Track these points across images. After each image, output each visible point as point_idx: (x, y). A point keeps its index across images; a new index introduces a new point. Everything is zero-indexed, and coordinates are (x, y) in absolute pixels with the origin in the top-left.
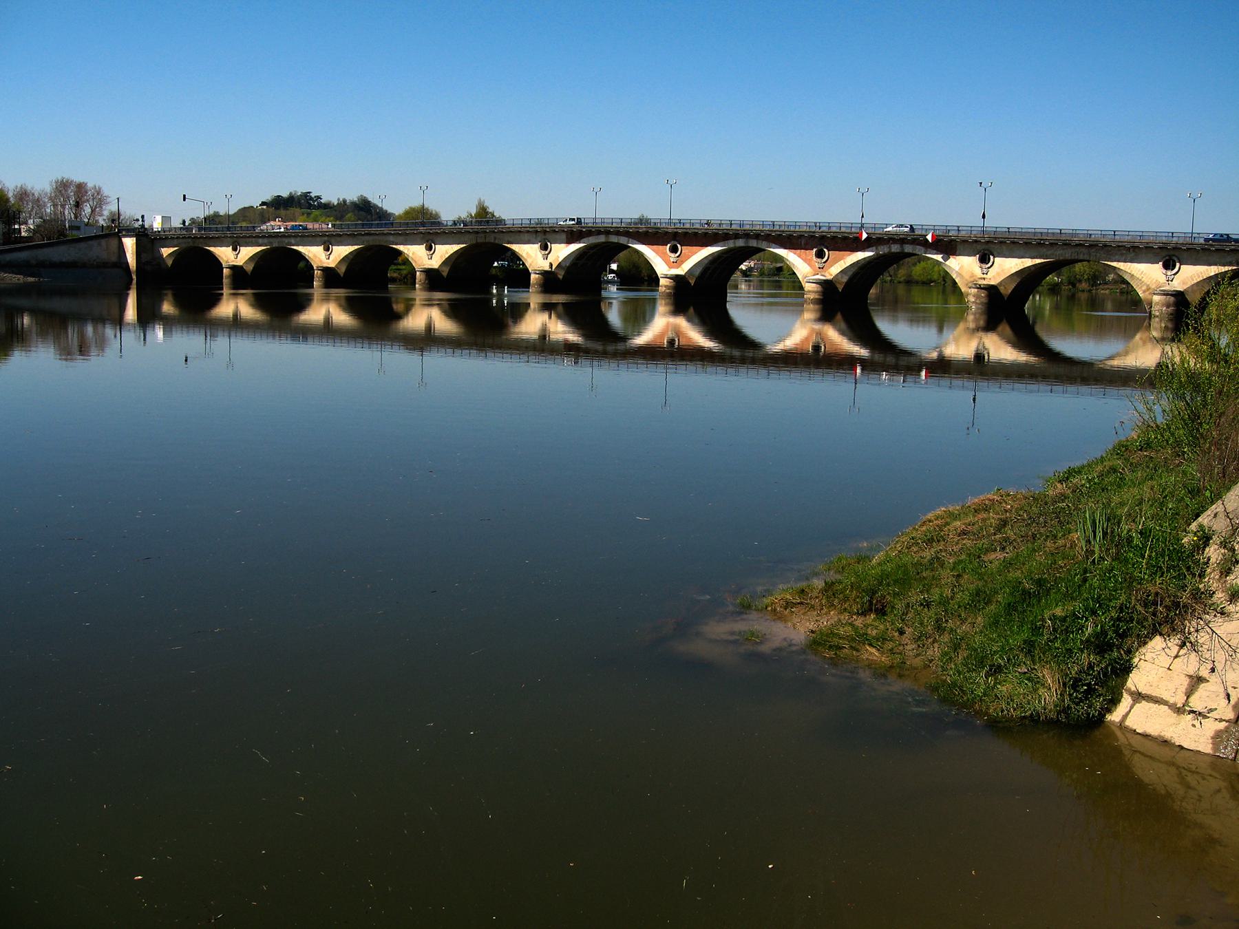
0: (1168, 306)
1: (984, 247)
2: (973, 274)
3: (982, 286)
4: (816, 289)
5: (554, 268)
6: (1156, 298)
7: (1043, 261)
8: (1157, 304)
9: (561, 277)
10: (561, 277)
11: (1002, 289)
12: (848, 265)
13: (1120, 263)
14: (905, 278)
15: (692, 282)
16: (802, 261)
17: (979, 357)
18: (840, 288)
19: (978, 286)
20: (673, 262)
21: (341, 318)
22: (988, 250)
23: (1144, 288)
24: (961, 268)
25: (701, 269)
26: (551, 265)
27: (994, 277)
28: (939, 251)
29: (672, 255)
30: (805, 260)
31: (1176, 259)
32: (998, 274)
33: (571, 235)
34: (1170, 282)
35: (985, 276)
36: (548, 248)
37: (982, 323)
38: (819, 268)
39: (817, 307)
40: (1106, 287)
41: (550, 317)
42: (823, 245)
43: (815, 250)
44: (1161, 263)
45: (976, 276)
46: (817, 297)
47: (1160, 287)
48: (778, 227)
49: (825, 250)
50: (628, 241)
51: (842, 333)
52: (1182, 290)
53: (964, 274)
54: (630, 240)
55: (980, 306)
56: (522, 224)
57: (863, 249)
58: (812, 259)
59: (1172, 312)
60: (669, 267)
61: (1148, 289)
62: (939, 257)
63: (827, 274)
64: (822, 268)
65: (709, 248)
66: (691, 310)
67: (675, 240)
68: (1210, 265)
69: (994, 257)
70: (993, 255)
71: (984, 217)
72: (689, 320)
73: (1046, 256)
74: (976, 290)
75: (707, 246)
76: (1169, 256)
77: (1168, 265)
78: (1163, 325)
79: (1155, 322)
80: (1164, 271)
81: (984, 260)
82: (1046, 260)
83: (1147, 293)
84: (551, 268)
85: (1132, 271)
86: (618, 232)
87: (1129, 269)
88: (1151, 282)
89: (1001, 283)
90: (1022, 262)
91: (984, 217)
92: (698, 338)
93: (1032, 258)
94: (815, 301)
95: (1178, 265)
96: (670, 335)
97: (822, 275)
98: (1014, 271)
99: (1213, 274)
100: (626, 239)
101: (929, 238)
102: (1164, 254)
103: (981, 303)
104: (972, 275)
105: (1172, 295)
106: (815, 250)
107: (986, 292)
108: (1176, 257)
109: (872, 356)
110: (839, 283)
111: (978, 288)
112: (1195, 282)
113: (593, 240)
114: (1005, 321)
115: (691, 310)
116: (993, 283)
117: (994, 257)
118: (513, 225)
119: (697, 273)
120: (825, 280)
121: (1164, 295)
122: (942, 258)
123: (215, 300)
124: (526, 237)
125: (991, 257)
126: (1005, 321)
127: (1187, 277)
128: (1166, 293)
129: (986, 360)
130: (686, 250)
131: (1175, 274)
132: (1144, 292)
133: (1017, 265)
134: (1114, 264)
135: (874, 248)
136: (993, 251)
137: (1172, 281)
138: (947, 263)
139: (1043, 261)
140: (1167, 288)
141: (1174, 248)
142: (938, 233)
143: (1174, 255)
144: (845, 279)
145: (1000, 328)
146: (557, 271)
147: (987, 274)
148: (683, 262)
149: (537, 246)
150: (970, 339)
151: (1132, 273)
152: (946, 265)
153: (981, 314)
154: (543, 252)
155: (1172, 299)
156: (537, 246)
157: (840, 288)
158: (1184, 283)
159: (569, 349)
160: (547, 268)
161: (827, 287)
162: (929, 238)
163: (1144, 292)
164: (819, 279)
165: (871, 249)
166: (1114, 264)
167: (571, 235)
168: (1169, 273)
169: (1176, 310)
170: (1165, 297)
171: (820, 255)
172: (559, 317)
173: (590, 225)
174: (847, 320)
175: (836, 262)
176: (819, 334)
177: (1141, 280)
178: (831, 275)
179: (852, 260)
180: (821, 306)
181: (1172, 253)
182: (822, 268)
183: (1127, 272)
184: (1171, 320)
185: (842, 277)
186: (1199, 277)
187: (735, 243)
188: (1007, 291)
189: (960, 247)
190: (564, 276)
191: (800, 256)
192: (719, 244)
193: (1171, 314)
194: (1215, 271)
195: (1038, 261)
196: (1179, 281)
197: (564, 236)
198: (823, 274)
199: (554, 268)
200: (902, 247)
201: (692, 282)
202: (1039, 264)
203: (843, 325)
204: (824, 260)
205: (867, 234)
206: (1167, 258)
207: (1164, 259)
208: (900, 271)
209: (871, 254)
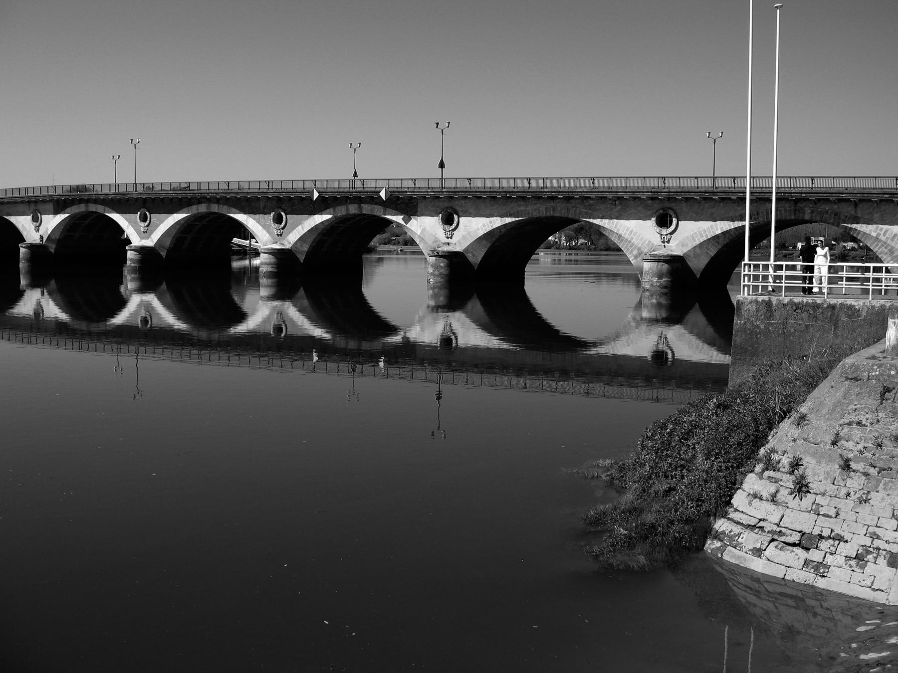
0: (660, 276)
1: (446, 204)
2: (436, 238)
3: (440, 254)
4: (268, 261)
5: (44, 241)
6: (647, 266)
7: (514, 219)
8: (647, 273)
9: (53, 251)
10: (53, 251)
11: (469, 256)
12: (306, 230)
13: (604, 220)
14: (605, 246)
15: (163, 254)
16: (261, 228)
17: (447, 341)
18: (302, 258)
19: (436, 254)
20: (144, 232)
21: (53, 311)
22: (451, 208)
23: (635, 252)
24: (424, 230)
25: (171, 239)
26: (42, 238)
27: (459, 241)
28: (399, 211)
29: (142, 224)
30: (264, 227)
31: (671, 213)
32: (464, 237)
33: (58, 204)
34: (666, 244)
35: (449, 241)
36: (282, 220)
37: (442, 300)
38: (278, 235)
39: (274, 280)
40: (758, 251)
41: (43, 294)
42: (280, 208)
43: (273, 214)
44: (654, 219)
45: (440, 241)
46: (270, 269)
47: (654, 251)
48: (275, 190)
49: (282, 213)
50: (105, 210)
51: (301, 310)
52: (681, 254)
53: (426, 238)
54: (107, 208)
55: (439, 279)
56: (376, 188)
57: (319, 211)
58: (269, 226)
59: (664, 284)
60: (141, 239)
61: (640, 254)
62: (398, 219)
63: (286, 243)
64: (281, 235)
65: (316, 216)
66: (164, 286)
67: (144, 207)
68: (715, 220)
69: (459, 217)
70: (457, 214)
71: (442, 165)
72: (160, 299)
73: (518, 212)
74: (434, 258)
75: (173, 214)
76: (664, 209)
77: (663, 222)
78: (654, 301)
79: (263, 281)
80: (658, 229)
81: (448, 220)
82: (517, 219)
83: (639, 259)
84: (42, 241)
85: (618, 230)
86: (96, 201)
87: (615, 227)
88: (642, 245)
89: (467, 249)
90: (491, 222)
91: (442, 165)
92: (168, 318)
93: (502, 216)
94: (270, 275)
95: (675, 221)
96: (143, 313)
97: (281, 244)
98: (481, 233)
99: (719, 232)
100: (103, 207)
101: (383, 194)
102: (657, 206)
103: (441, 275)
104: (436, 240)
105: (665, 261)
106: (273, 214)
107: (446, 260)
108: (673, 210)
109: (333, 339)
110: (299, 252)
111: (435, 256)
112: (698, 243)
113: (196, 209)
114: (475, 296)
115: (164, 286)
116: (458, 249)
117: (459, 217)
118: (304, 189)
119: (168, 243)
120: (278, 250)
121: (655, 261)
122: (403, 219)
123: (18, 295)
124: (21, 208)
125: (456, 217)
126: (475, 296)
127: (687, 238)
128: (657, 259)
129: (454, 345)
130: (155, 217)
131: (671, 233)
132: (636, 257)
133: (484, 225)
134: (597, 222)
135: (331, 210)
136: (457, 208)
137: (668, 242)
138: (407, 226)
139: (514, 219)
140: (662, 252)
141: (669, 199)
142: (392, 184)
143: (670, 208)
144: (306, 248)
145: (469, 305)
146: (48, 244)
147: (451, 238)
148: (152, 232)
149: (30, 218)
150: (436, 320)
151: (620, 232)
152: (407, 228)
153: (440, 288)
154: (448, 228)
155: (665, 267)
156: (30, 218)
157: (302, 258)
158: (683, 245)
159: (60, 328)
160: (38, 241)
161: (283, 257)
162: (383, 194)
163: (636, 257)
164: (272, 249)
165: (328, 210)
166: (597, 222)
167: (58, 204)
168: (665, 231)
169: (671, 281)
170: (656, 263)
171: (278, 220)
172: (50, 294)
173: (346, 190)
174: (310, 295)
175: (294, 227)
176: (280, 313)
177: (630, 242)
178: (290, 243)
179: (309, 225)
180: (275, 280)
181: (667, 205)
182: (281, 235)
183: (614, 232)
184: (665, 294)
185: (301, 246)
186: (702, 236)
187: (208, 208)
188: (698, 265)
189: (421, 206)
190: (56, 249)
191: (258, 222)
192: (185, 209)
193: (665, 287)
194: (722, 228)
195: (509, 220)
196: (678, 242)
197: (50, 206)
198: (282, 242)
199: (44, 241)
200: (87, 206)
201: (163, 254)
202: (509, 223)
203: (305, 302)
204: (282, 225)
205: (318, 192)
206: (661, 212)
207: (658, 214)
208: (600, 241)
209: (329, 217)
